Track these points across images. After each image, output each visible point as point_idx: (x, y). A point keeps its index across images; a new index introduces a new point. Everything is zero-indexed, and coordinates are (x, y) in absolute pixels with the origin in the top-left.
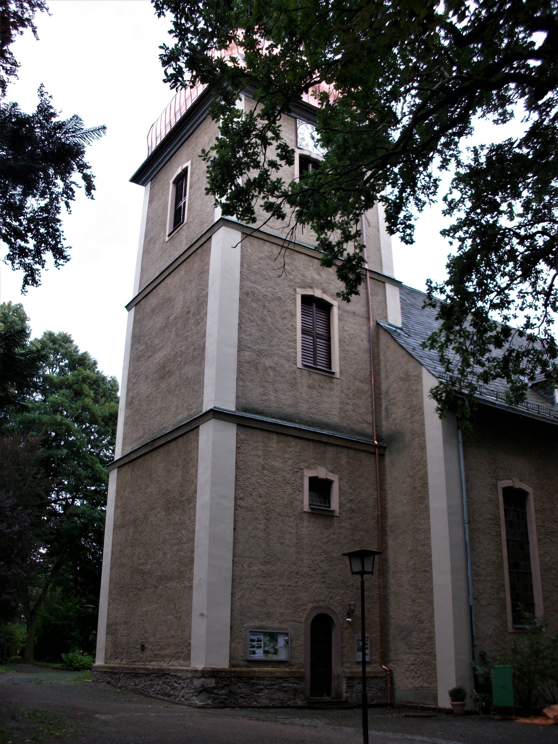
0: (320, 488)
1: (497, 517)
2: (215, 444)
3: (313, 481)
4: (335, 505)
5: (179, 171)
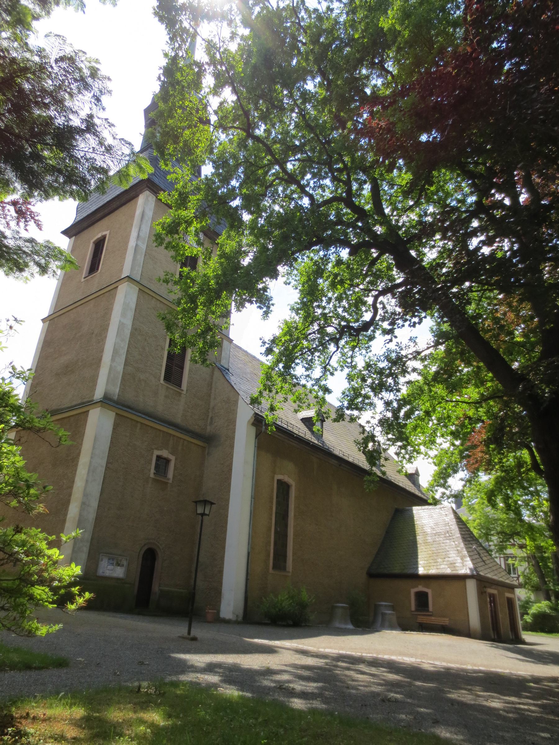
0: (162, 464)
1: (271, 498)
2: (99, 425)
3: (159, 457)
4: (170, 474)
5: (99, 235)
